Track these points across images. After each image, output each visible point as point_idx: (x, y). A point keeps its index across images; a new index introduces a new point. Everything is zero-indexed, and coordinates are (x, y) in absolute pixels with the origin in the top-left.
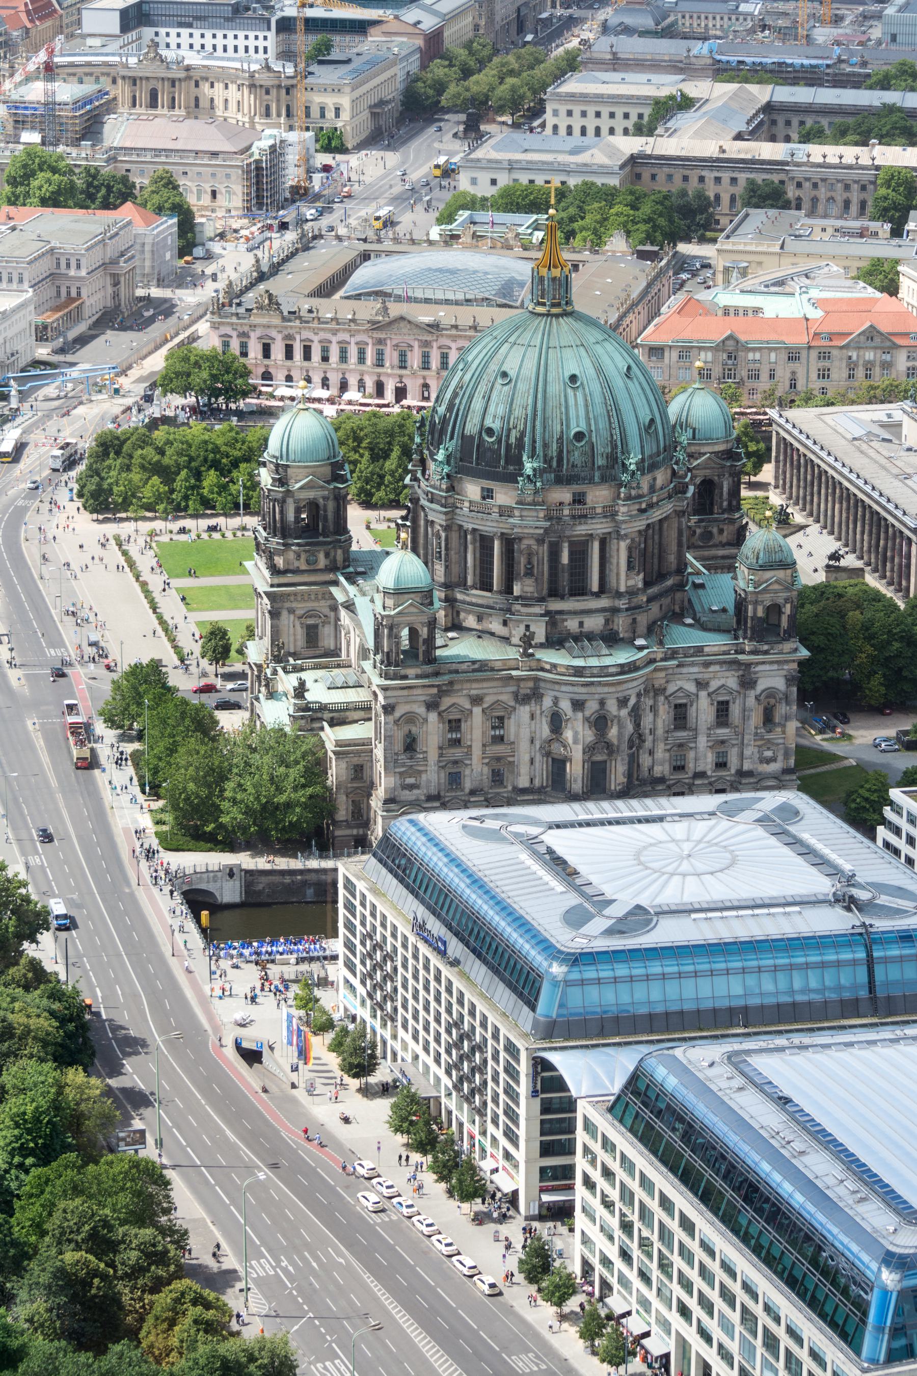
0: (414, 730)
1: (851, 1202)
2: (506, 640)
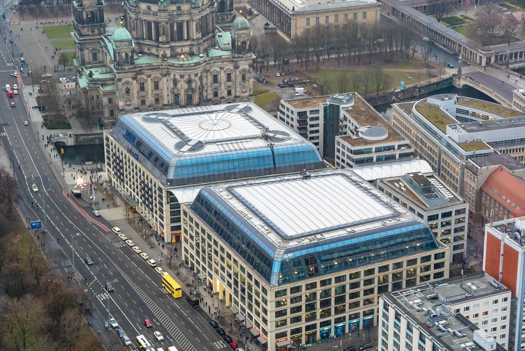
0: (129, 87)
1: (266, 233)
2: (157, 56)
